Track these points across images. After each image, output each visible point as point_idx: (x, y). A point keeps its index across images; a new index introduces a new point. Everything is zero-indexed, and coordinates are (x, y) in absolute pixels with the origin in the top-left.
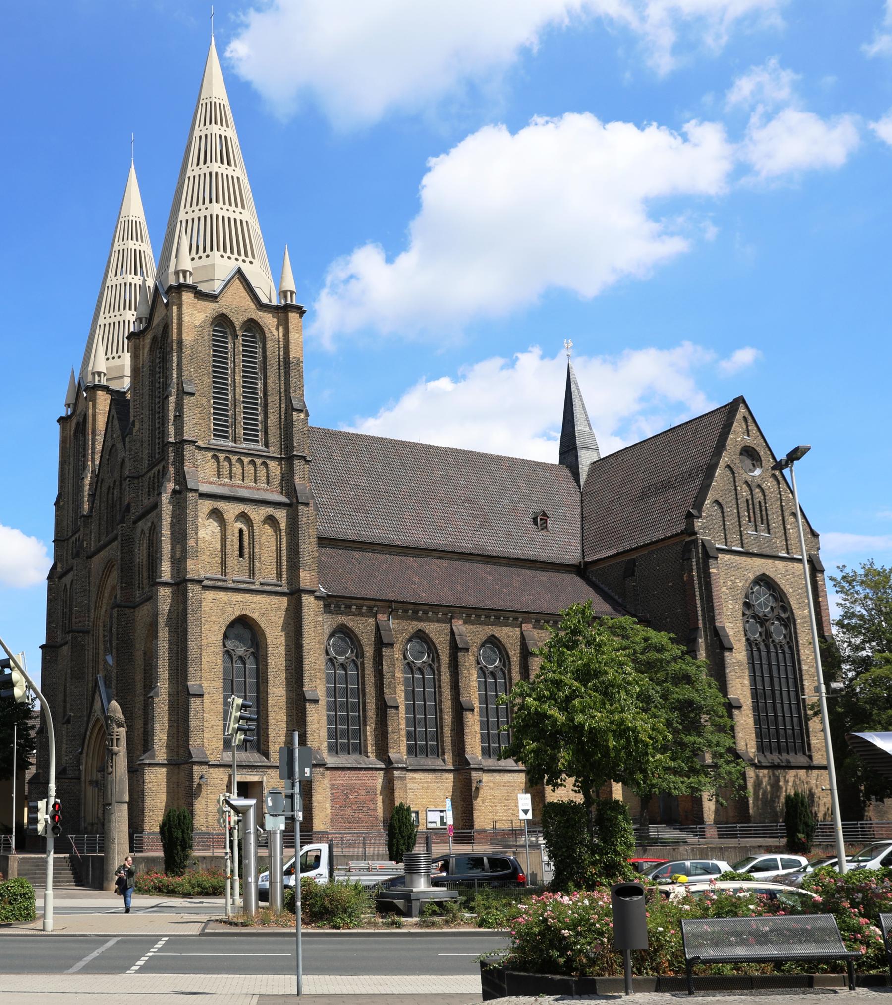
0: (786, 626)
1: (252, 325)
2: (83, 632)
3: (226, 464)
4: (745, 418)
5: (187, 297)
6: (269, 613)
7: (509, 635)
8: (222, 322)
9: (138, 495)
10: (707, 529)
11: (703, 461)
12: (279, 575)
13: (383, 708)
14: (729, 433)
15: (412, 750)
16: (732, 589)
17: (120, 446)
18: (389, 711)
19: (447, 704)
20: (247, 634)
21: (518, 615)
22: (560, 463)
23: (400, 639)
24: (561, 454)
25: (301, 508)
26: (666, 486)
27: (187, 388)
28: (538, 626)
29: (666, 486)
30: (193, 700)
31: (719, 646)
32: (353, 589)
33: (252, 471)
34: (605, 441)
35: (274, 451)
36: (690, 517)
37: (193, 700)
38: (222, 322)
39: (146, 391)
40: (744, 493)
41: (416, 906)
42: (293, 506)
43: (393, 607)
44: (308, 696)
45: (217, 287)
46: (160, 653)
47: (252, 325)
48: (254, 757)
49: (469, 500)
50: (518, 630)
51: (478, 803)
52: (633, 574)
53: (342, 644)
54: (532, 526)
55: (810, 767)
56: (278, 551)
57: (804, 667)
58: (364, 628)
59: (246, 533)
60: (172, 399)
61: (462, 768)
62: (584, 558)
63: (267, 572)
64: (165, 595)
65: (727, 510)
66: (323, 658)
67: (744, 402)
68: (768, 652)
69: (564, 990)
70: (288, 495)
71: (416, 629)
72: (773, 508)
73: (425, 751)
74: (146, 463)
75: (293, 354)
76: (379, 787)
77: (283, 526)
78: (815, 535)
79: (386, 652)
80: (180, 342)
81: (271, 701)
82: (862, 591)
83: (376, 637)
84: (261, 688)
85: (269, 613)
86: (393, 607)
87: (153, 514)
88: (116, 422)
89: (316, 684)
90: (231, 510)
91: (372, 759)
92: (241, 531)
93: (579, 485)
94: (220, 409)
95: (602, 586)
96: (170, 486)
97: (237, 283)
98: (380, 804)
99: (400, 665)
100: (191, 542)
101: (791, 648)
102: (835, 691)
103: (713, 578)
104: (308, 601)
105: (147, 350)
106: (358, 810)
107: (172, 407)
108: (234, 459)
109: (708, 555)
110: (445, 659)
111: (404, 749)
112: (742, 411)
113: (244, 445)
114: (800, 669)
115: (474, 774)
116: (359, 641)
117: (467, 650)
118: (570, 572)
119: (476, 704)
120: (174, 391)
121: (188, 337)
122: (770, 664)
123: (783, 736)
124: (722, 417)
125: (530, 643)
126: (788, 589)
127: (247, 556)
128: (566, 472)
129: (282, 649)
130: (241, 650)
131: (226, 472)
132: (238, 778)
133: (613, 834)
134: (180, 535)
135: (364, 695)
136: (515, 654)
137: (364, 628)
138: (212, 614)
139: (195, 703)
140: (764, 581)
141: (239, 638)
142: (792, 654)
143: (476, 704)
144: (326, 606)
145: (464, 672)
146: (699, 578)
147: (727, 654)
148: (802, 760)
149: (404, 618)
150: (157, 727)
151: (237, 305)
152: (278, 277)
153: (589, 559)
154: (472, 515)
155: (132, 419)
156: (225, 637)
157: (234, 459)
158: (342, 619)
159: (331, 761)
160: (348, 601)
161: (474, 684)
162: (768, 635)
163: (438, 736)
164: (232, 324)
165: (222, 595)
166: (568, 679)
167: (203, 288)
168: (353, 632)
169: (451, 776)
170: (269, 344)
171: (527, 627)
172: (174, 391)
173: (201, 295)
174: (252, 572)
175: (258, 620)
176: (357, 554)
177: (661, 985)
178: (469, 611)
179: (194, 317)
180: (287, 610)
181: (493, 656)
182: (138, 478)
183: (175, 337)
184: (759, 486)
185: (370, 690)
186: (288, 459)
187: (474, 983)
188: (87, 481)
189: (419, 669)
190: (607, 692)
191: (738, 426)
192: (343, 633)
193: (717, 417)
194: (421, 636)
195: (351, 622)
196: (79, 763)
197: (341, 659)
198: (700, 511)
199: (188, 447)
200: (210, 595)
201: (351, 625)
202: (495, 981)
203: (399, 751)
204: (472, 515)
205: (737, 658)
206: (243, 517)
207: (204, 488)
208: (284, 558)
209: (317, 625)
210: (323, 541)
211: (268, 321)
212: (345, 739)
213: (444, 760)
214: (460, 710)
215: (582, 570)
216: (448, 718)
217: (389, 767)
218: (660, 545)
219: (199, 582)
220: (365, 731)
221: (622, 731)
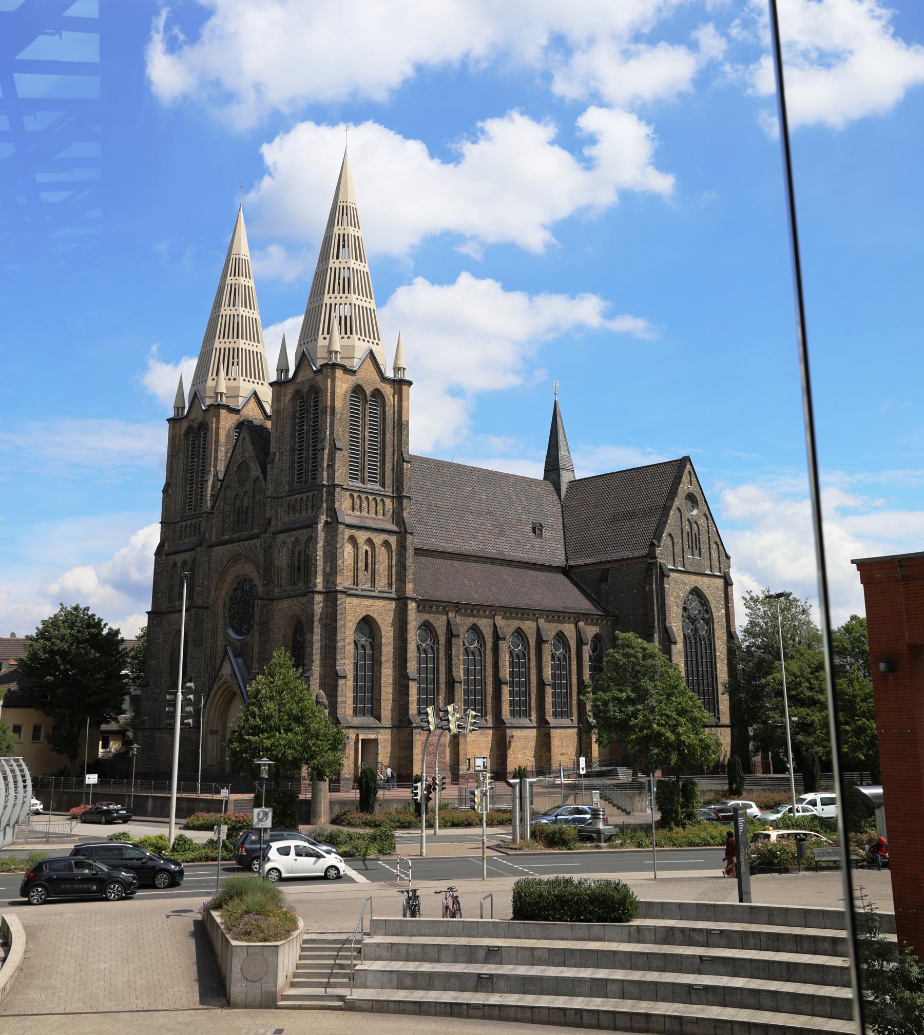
0: (707, 624)
2: (203, 608)
3: (358, 500)
4: (690, 472)
5: (339, 373)
7: (529, 627)
8: (358, 390)
9: (277, 512)
11: (661, 503)
14: (679, 483)
16: (677, 598)
18: (456, 685)
19: (490, 679)
21: (536, 612)
22: (545, 478)
23: (462, 630)
24: (546, 471)
25: (408, 536)
26: (632, 515)
29: (632, 515)
30: (340, 680)
31: (668, 641)
32: (440, 594)
33: (374, 506)
35: (388, 491)
36: (652, 545)
37: (340, 680)
38: (358, 390)
40: (687, 528)
41: (602, 836)
43: (459, 607)
46: (315, 644)
47: (377, 393)
48: (369, 720)
49: (489, 513)
50: (535, 623)
52: (607, 580)
53: (424, 634)
55: (717, 726)
57: (718, 654)
58: (439, 622)
59: (370, 553)
60: (326, 451)
62: (567, 561)
63: (382, 583)
65: (676, 540)
67: (690, 460)
68: (696, 643)
69: (780, 871)
70: (397, 525)
71: (472, 623)
72: (704, 538)
74: (286, 489)
76: (448, 741)
77: (394, 548)
78: (728, 557)
79: (454, 641)
80: (333, 408)
81: (383, 679)
82: (762, 609)
83: (447, 629)
84: (376, 669)
85: (383, 613)
90: (362, 536)
92: (366, 551)
93: (559, 495)
95: (582, 585)
96: (323, 518)
98: (448, 754)
99: (462, 650)
100: (340, 563)
101: (709, 640)
102: (793, 722)
103: (666, 590)
104: (412, 605)
105: (288, 397)
107: (326, 457)
109: (663, 575)
110: (489, 645)
113: (369, 486)
114: (715, 655)
115: (508, 731)
116: (436, 632)
117: (504, 639)
118: (558, 572)
121: (338, 404)
122: (696, 652)
125: (543, 633)
127: (370, 571)
128: (550, 487)
129: (391, 640)
130: (363, 641)
131: (357, 507)
132: (361, 737)
133: (692, 798)
134: (332, 556)
135: (438, 673)
138: (351, 611)
139: (341, 683)
140: (696, 592)
142: (710, 644)
144: (418, 606)
146: (657, 590)
147: (673, 646)
149: (464, 615)
153: (572, 563)
154: (493, 525)
155: (272, 450)
157: (363, 496)
158: (426, 616)
160: (431, 603)
162: (696, 630)
164: (364, 392)
167: (345, 362)
168: (432, 626)
169: (490, 732)
170: (387, 409)
174: (373, 583)
175: (377, 619)
178: (506, 610)
180: (395, 611)
181: (518, 642)
182: (277, 498)
183: (329, 403)
184: (696, 522)
185: (443, 669)
186: (399, 498)
188: (210, 483)
189: (472, 652)
191: (685, 478)
192: (427, 628)
194: (475, 629)
195: (431, 618)
197: (424, 645)
198: (659, 542)
199: (338, 490)
200: (349, 600)
201: (431, 620)
204: (493, 525)
205: (678, 649)
206: (369, 541)
207: (348, 520)
208: (394, 573)
210: (419, 552)
211: (387, 390)
212: (520, 710)
213: (486, 720)
215: (566, 571)
216: (490, 689)
218: (628, 562)
220: (438, 699)
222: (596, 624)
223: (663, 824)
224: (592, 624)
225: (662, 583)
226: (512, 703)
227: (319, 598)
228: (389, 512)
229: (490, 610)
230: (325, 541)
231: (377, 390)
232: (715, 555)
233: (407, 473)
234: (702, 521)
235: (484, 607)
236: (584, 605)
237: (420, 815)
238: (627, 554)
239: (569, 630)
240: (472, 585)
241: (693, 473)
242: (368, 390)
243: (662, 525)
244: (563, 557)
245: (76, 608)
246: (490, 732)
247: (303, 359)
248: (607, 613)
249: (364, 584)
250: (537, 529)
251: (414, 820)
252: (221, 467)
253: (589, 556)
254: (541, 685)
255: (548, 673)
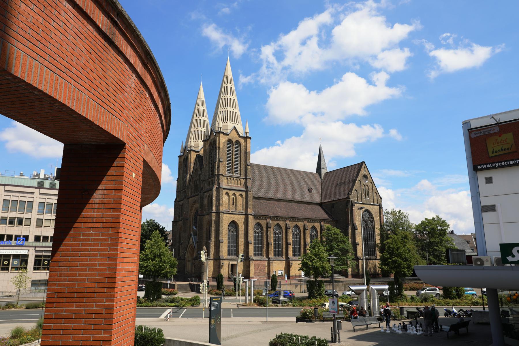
1: (238, 142)
5: (221, 135)
6: (240, 220)
7: (300, 224)
8: (230, 141)
10: (353, 198)
11: (353, 178)
12: (243, 210)
13: (268, 244)
15: (275, 255)
17: (199, 170)
19: (284, 243)
20: (234, 225)
26: (343, 184)
27: (221, 160)
28: (308, 222)
29: (343, 184)
31: (354, 228)
34: (330, 166)
35: (242, 176)
36: (348, 194)
38: (230, 141)
39: (208, 156)
40: (363, 187)
42: (247, 192)
43: (271, 218)
44: (250, 242)
45: (229, 131)
47: (238, 142)
49: (291, 184)
51: (291, 269)
54: (308, 192)
55: (375, 260)
56: (243, 203)
58: (263, 223)
60: (217, 163)
61: (288, 260)
63: (240, 209)
64: (214, 216)
65: (358, 192)
66: (253, 231)
69: (307, 321)
73: (278, 255)
75: (248, 150)
77: (244, 196)
78: (381, 198)
80: (219, 147)
81: (240, 243)
85: (240, 220)
86: (271, 218)
87: (210, 192)
88: (198, 163)
89: (251, 239)
90: (231, 193)
91: (265, 257)
93: (321, 178)
94: (229, 166)
96: (216, 186)
97: (234, 130)
99: (272, 232)
100: (221, 202)
104: (250, 217)
106: (261, 271)
107: (216, 165)
108: (232, 178)
109: (353, 205)
110: (284, 231)
111: (273, 255)
112: (364, 165)
119: (292, 243)
120: (217, 160)
121: (221, 146)
123: (370, 251)
124: (358, 167)
126: (373, 213)
128: (318, 175)
129: (243, 229)
130: (232, 229)
131: (230, 182)
134: (218, 200)
136: (302, 229)
137: (263, 223)
138: (226, 220)
139: (221, 244)
140: (367, 211)
141: (232, 226)
143: (292, 243)
144: (254, 217)
145: (289, 234)
148: (374, 258)
150: (211, 250)
151: (234, 137)
152: (245, 128)
156: (229, 226)
157: (232, 178)
158: (258, 221)
159: (254, 258)
161: (291, 237)
162: (367, 225)
163: (282, 251)
165: (228, 215)
166: (313, 256)
167: (225, 132)
169: (284, 262)
171: (305, 222)
172: (217, 160)
173: (224, 134)
174: (236, 209)
176: (262, 201)
177: (320, 321)
179: (223, 140)
185: (265, 239)
186: (246, 179)
187: (294, 319)
188: (188, 177)
190: (320, 259)
192: (259, 225)
193: (357, 166)
194: (278, 225)
196: (185, 255)
199: (220, 176)
200: (225, 215)
202: (298, 320)
203: (271, 256)
206: (234, 194)
207: (224, 187)
209: (252, 222)
210: (254, 198)
211: (242, 141)
212: (258, 252)
214: (287, 244)
215: (320, 205)
216: (284, 246)
217: (269, 260)
219: (223, 212)
221: (323, 267)
222: (329, 223)
223: (309, 298)
224: (327, 223)
225: (352, 208)
226: (293, 252)
227: (214, 215)
228: (243, 184)
229: (285, 219)
230: (216, 195)
231: (237, 141)
232: (375, 197)
233: (249, 170)
234: (370, 185)
235: (282, 217)
236: (325, 216)
237: (236, 291)
238: (341, 198)
239: (317, 225)
240: (279, 210)
241: (366, 167)
242: (234, 141)
243: (353, 186)
244: (320, 200)
245: (151, 220)
246: (284, 262)
247: (212, 131)
248: (333, 220)
249: (232, 209)
250: (310, 190)
251: (232, 292)
252: (191, 171)
253: (328, 199)
254: (305, 245)
255: (308, 240)
